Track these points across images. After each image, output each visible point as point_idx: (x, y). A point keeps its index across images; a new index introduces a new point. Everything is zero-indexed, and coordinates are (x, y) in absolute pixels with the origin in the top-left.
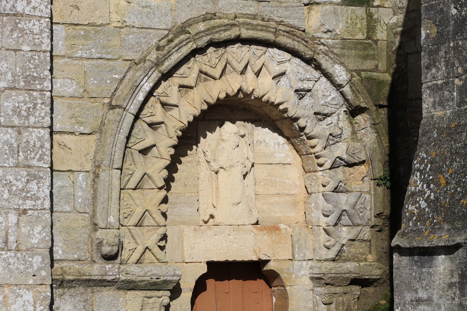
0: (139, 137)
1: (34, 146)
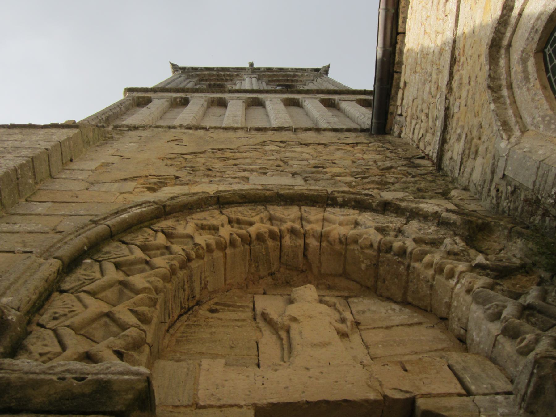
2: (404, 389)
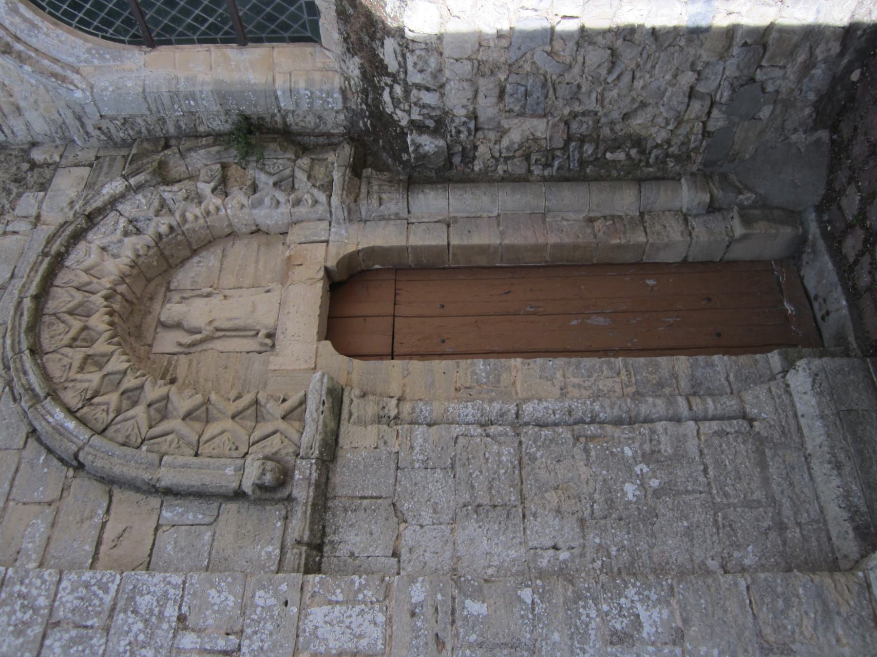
1: (82, 599)
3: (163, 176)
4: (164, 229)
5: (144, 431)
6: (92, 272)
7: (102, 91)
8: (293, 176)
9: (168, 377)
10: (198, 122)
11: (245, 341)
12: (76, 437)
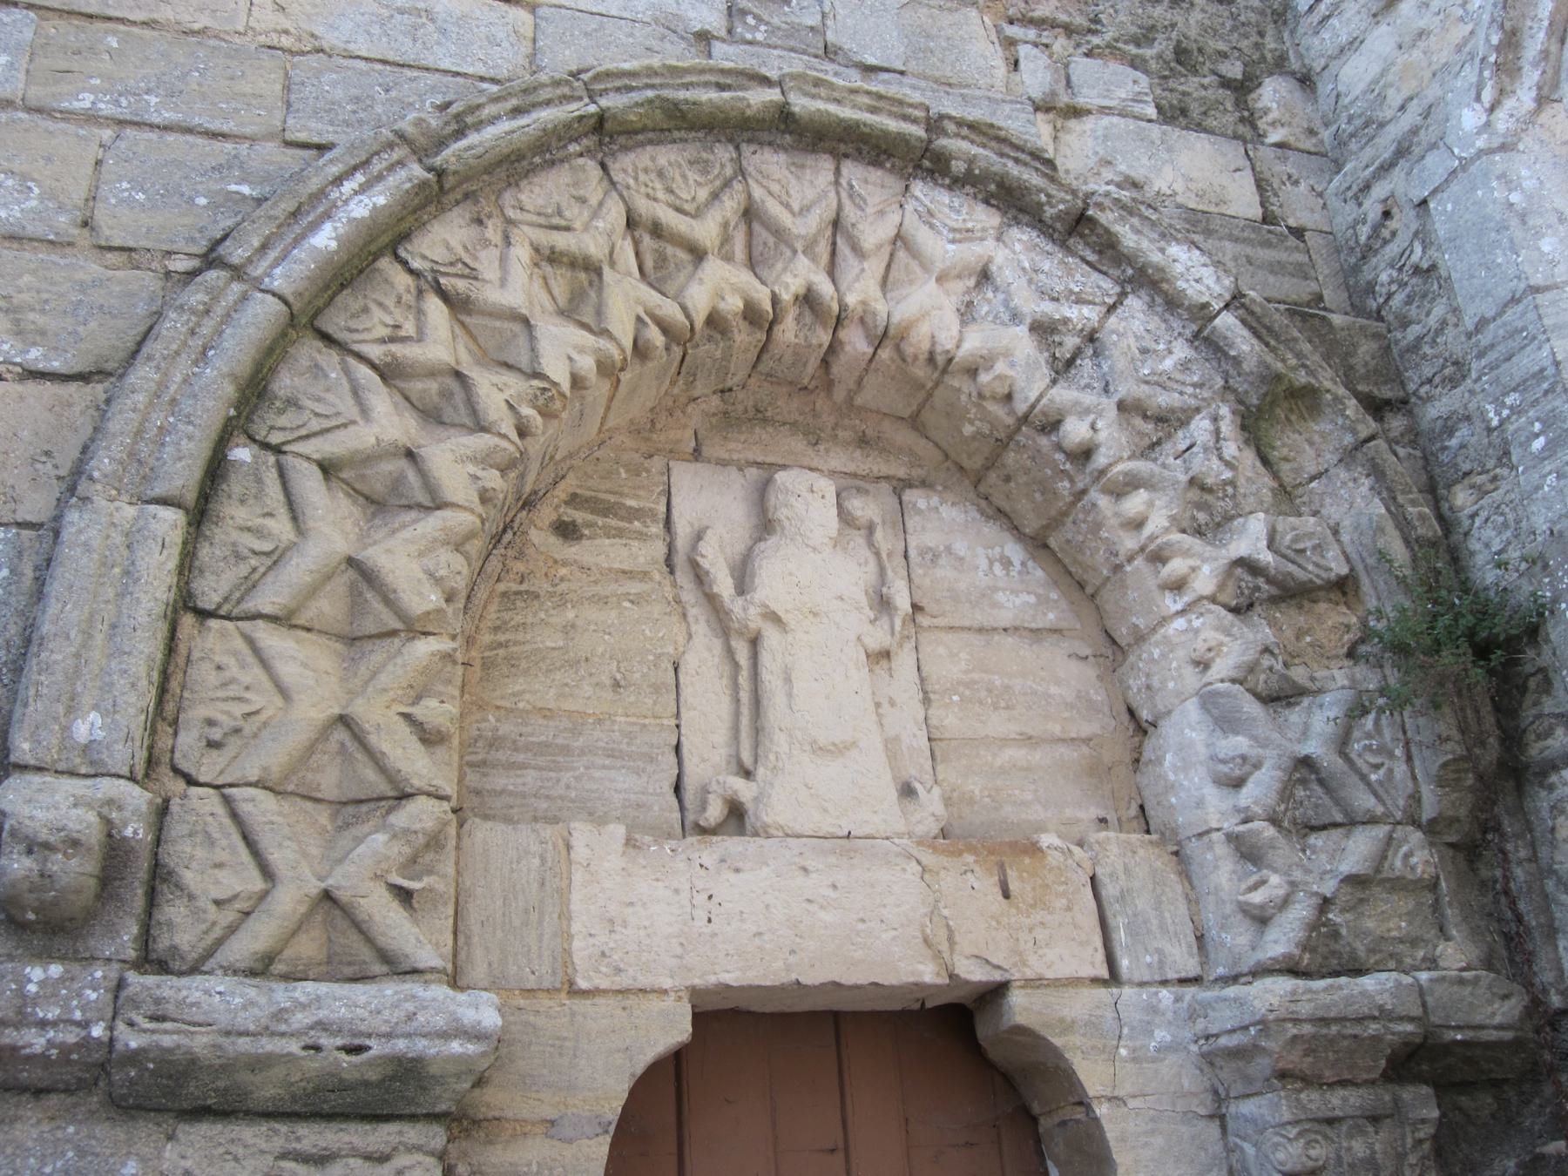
0: (320, 409)
2: (995, 961)
3: (1267, 410)
4: (1075, 431)
5: (313, 448)
6: (901, 254)
7: (1502, 177)
8: (1351, 822)
9: (579, 516)
10: (1479, 479)
11: (721, 736)
12: (284, 257)
